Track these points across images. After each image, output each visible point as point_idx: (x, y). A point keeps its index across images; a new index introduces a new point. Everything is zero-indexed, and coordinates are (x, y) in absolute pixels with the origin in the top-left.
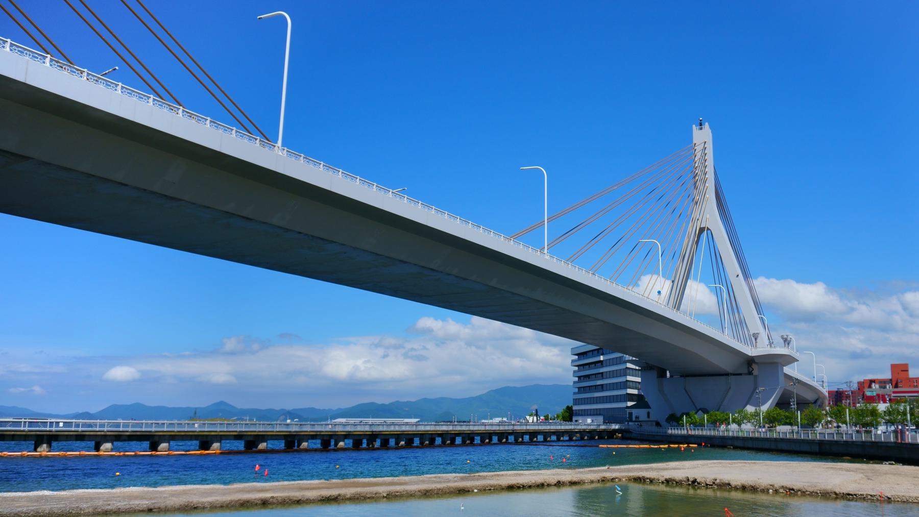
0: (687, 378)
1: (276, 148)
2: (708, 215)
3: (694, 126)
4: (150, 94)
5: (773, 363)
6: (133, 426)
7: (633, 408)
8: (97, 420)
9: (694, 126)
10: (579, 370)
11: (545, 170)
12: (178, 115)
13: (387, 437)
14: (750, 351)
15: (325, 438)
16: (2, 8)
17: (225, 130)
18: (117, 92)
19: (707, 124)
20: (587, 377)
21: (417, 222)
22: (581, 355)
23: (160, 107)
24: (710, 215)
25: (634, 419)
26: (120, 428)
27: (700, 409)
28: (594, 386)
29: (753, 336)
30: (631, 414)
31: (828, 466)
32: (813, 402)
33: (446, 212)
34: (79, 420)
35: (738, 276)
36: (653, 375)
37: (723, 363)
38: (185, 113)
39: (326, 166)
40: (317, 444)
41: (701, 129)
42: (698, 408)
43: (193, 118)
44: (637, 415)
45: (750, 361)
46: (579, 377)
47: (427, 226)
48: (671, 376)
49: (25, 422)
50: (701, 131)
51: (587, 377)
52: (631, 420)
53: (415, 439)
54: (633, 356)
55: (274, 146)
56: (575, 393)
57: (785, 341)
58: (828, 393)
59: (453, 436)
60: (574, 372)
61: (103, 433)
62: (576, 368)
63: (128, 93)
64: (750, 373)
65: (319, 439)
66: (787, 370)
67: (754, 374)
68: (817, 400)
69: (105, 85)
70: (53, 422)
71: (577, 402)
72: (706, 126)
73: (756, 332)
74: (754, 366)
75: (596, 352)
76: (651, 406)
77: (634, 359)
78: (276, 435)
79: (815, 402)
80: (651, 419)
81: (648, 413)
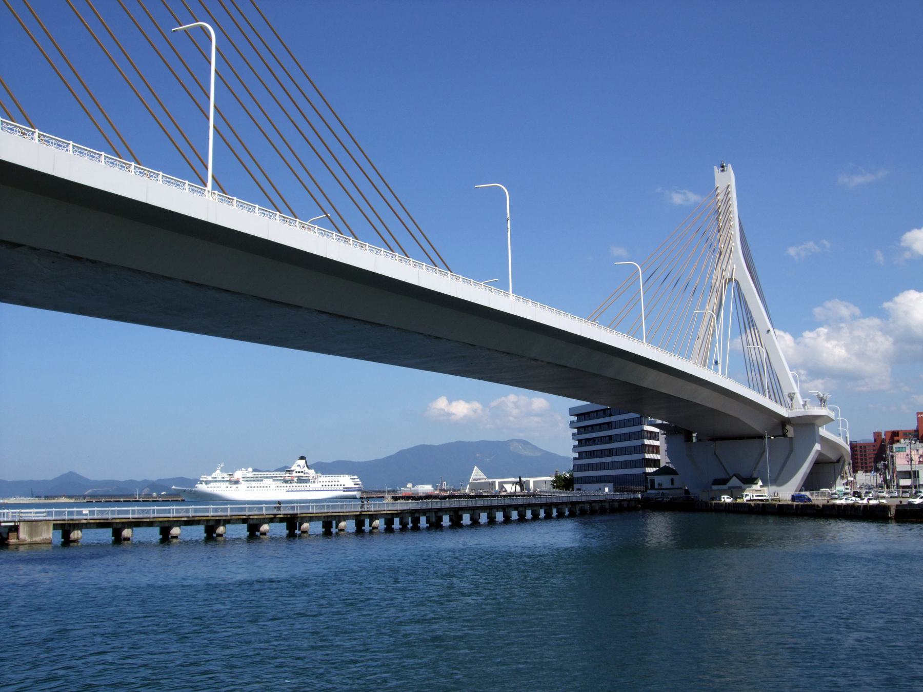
0: (717, 442)
1: (206, 192)
2: (735, 265)
3: (715, 168)
4: (185, 180)
5: (808, 424)
6: (138, 513)
7: (655, 475)
8: (227, 505)
9: (715, 168)
10: (579, 433)
11: (637, 264)
12: (255, 214)
13: (329, 520)
14: (784, 412)
15: (211, 523)
16: (2, 83)
17: (91, 156)
18: (68, 152)
19: (730, 166)
20: (593, 441)
21: (125, 198)
22: (582, 416)
23: (9, 131)
24: (737, 266)
25: (656, 487)
26: (74, 515)
27: (735, 475)
28: (599, 450)
29: (789, 396)
30: (653, 482)
31: (139, 650)
32: (835, 461)
33: (471, 280)
34: (65, 508)
35: (768, 331)
36: (680, 438)
37: (756, 425)
38: (42, 137)
39: (139, 168)
40: (199, 532)
41: (723, 171)
42: (731, 475)
43: (85, 154)
44: (660, 482)
45: (784, 422)
46: (580, 441)
47: (489, 308)
48: (699, 440)
49: (297, 506)
50: (723, 173)
51: (593, 441)
52: (653, 487)
53: (463, 515)
54: (663, 420)
55: (205, 190)
56: (575, 459)
57: (821, 401)
58: (851, 448)
59: (390, 517)
60: (574, 434)
61: (148, 520)
62: (576, 431)
63: (9, 129)
64: (785, 435)
65: (157, 526)
66: (823, 431)
67: (788, 436)
68: (840, 459)
69: (56, 146)
70: (313, 506)
71: (578, 468)
72: (730, 169)
73: (791, 392)
74: (788, 427)
75: (602, 412)
76: (678, 472)
77: (665, 422)
78: (387, 514)
79: (838, 461)
80: (674, 487)
81: (672, 480)
